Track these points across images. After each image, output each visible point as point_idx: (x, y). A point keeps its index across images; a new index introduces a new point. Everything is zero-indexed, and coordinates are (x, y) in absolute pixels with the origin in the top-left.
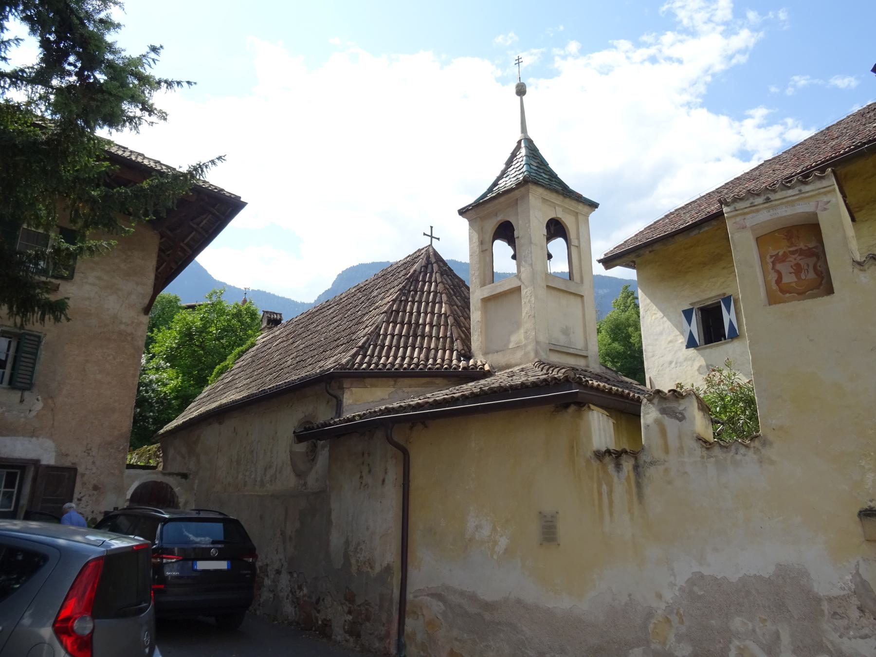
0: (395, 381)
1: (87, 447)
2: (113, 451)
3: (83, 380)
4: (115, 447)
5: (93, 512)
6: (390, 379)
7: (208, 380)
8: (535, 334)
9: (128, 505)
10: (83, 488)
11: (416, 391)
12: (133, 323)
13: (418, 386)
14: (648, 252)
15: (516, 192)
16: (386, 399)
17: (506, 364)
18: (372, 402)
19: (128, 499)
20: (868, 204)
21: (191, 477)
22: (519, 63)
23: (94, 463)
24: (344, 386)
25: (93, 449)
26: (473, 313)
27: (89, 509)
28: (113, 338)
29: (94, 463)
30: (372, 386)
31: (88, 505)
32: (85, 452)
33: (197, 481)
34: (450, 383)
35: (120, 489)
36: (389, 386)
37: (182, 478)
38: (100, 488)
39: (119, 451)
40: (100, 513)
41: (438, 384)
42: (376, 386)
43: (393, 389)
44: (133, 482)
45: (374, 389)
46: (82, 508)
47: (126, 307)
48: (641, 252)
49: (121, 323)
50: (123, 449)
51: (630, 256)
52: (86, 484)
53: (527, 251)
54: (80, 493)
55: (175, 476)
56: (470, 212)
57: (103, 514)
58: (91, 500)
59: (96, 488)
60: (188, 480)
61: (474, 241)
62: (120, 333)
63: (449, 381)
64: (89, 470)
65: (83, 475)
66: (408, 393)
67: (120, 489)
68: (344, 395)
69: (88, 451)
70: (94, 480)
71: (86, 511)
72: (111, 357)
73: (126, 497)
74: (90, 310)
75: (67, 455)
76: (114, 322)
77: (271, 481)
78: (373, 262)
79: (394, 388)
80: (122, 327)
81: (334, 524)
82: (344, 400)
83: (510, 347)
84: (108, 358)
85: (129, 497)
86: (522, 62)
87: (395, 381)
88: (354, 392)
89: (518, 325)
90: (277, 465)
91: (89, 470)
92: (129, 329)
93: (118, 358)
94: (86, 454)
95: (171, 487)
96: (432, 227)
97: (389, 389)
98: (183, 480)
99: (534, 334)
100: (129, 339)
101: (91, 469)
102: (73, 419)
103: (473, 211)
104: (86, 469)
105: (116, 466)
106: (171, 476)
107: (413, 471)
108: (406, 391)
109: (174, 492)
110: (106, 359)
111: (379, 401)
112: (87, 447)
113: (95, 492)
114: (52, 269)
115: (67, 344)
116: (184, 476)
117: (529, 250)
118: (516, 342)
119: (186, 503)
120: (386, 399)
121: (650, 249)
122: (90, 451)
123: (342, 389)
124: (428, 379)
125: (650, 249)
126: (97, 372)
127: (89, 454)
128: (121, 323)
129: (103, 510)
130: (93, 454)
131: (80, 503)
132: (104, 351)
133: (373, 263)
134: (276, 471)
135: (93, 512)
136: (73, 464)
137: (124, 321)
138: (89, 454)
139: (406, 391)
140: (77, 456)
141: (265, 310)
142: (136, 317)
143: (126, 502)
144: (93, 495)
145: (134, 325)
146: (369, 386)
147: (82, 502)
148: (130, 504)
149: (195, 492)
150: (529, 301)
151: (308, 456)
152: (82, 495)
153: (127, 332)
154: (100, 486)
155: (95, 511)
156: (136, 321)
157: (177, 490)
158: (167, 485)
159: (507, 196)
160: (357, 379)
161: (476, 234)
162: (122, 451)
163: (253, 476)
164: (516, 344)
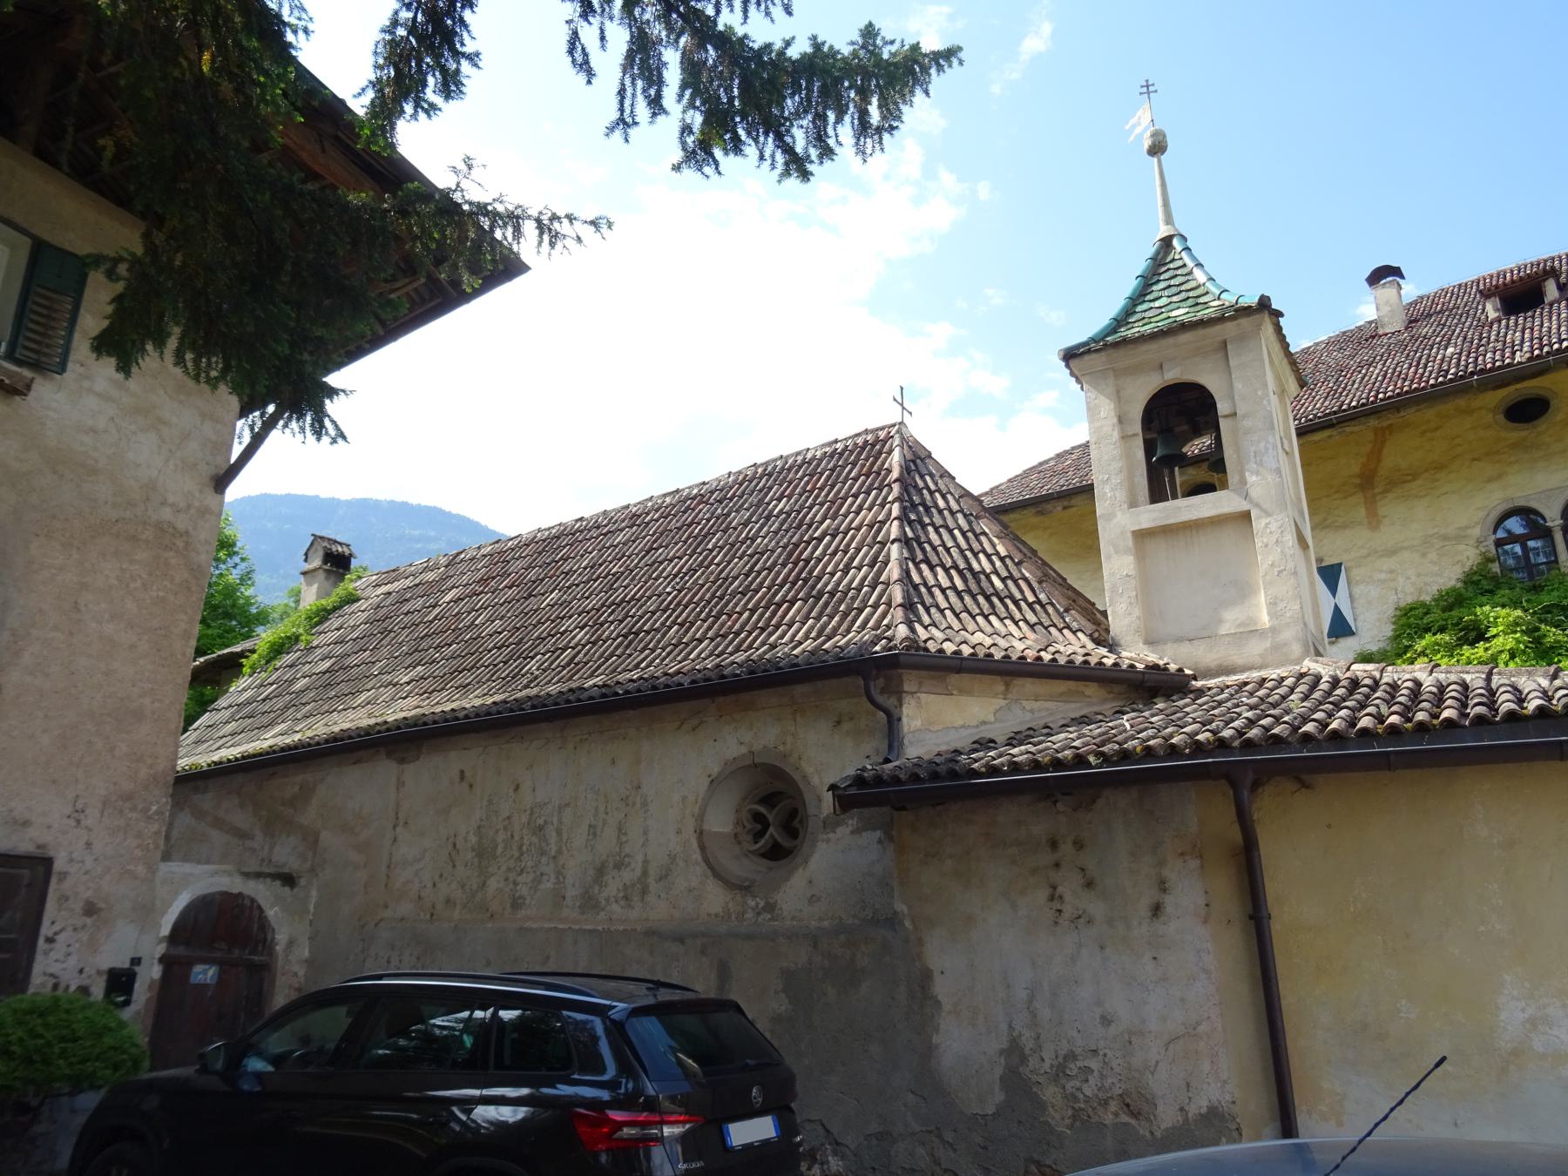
0: (1007, 685)
1: (74, 806)
2: (134, 815)
3: (71, 634)
4: (140, 806)
5: (81, 971)
6: (998, 678)
7: (242, 666)
8: (1301, 608)
9: (163, 951)
10: (59, 910)
11: (1048, 710)
12: (189, 507)
13: (1051, 698)
14: (1060, 509)
15: (1229, 325)
16: (991, 723)
17: (1220, 666)
18: (963, 727)
19: (165, 937)
20: (1426, 471)
21: (303, 882)
22: (1148, 93)
23: (89, 844)
24: (906, 687)
25: (88, 811)
26: (1109, 557)
27: (72, 962)
28: (144, 537)
29: (89, 844)
30: (962, 692)
31: (69, 955)
32: (69, 817)
33: (314, 893)
34: (1112, 695)
35: (146, 912)
36: (995, 696)
37: (284, 885)
38: (101, 909)
39: (149, 818)
40: (99, 972)
41: (1089, 697)
42: (969, 693)
43: (1003, 703)
44: (177, 893)
45: (963, 699)
46: (56, 961)
47: (176, 465)
48: (1048, 507)
49: (164, 503)
50: (156, 813)
51: (1025, 512)
52: (67, 899)
53: (1262, 444)
54: (53, 923)
55: (268, 880)
56: (1094, 356)
57: (105, 977)
58: (77, 941)
59: (90, 910)
60: (295, 890)
61: (1102, 414)
62: (160, 527)
63: (1109, 693)
64: (79, 862)
65: (63, 876)
66: (1032, 711)
67: (146, 912)
68: (904, 709)
69: (77, 815)
70: (88, 888)
71: (64, 969)
72: (138, 584)
73: (159, 933)
74: (96, 461)
75: (26, 824)
76: (148, 499)
77: (626, 898)
78: (289, 494)
79: (1005, 699)
80: (167, 514)
81: (947, 1007)
82: (905, 720)
83: (1222, 632)
84: (132, 585)
85: (166, 930)
86: (1156, 91)
87: (1007, 685)
88: (923, 701)
89: (1243, 592)
90: (646, 862)
91: (79, 862)
92: (182, 523)
93: (155, 588)
94: (72, 823)
95: (259, 907)
96: (902, 388)
97: (994, 700)
98: (287, 889)
99: (1297, 607)
100: (180, 543)
101: (83, 862)
102: (45, 731)
103: (1103, 354)
104: (71, 860)
105: (140, 854)
106: (261, 879)
107: (1273, 888)
108: (1028, 708)
109: (266, 917)
110: (127, 586)
111: (977, 726)
112: (74, 806)
113: (89, 921)
114: (8, 338)
115: (37, 535)
116: (289, 880)
117: (1268, 442)
118: (1239, 622)
119: (291, 943)
120: (991, 723)
121: (1066, 503)
122: (82, 816)
123: (899, 694)
124: (1071, 685)
125: (1066, 503)
126: (107, 616)
127: (78, 821)
128: (164, 503)
129: (105, 966)
130: (89, 822)
131: (51, 950)
132: (124, 566)
133: (288, 495)
134: (645, 873)
135: (81, 971)
136: (39, 847)
137: (171, 499)
138: (78, 821)
139: (1028, 708)
140: (49, 827)
141: (317, 534)
142: (197, 495)
143: (158, 944)
144: (84, 927)
145: (193, 511)
146: (955, 692)
147: (56, 945)
148: (168, 949)
149: (311, 917)
150: (1277, 541)
151: (739, 843)
152: (56, 928)
153: (175, 528)
154: (102, 905)
155: (86, 970)
156: (197, 504)
157: (272, 913)
158: (253, 900)
159: (1201, 332)
160: (932, 673)
161: (1108, 401)
162: (156, 817)
163: (548, 885)
164: (1240, 625)
